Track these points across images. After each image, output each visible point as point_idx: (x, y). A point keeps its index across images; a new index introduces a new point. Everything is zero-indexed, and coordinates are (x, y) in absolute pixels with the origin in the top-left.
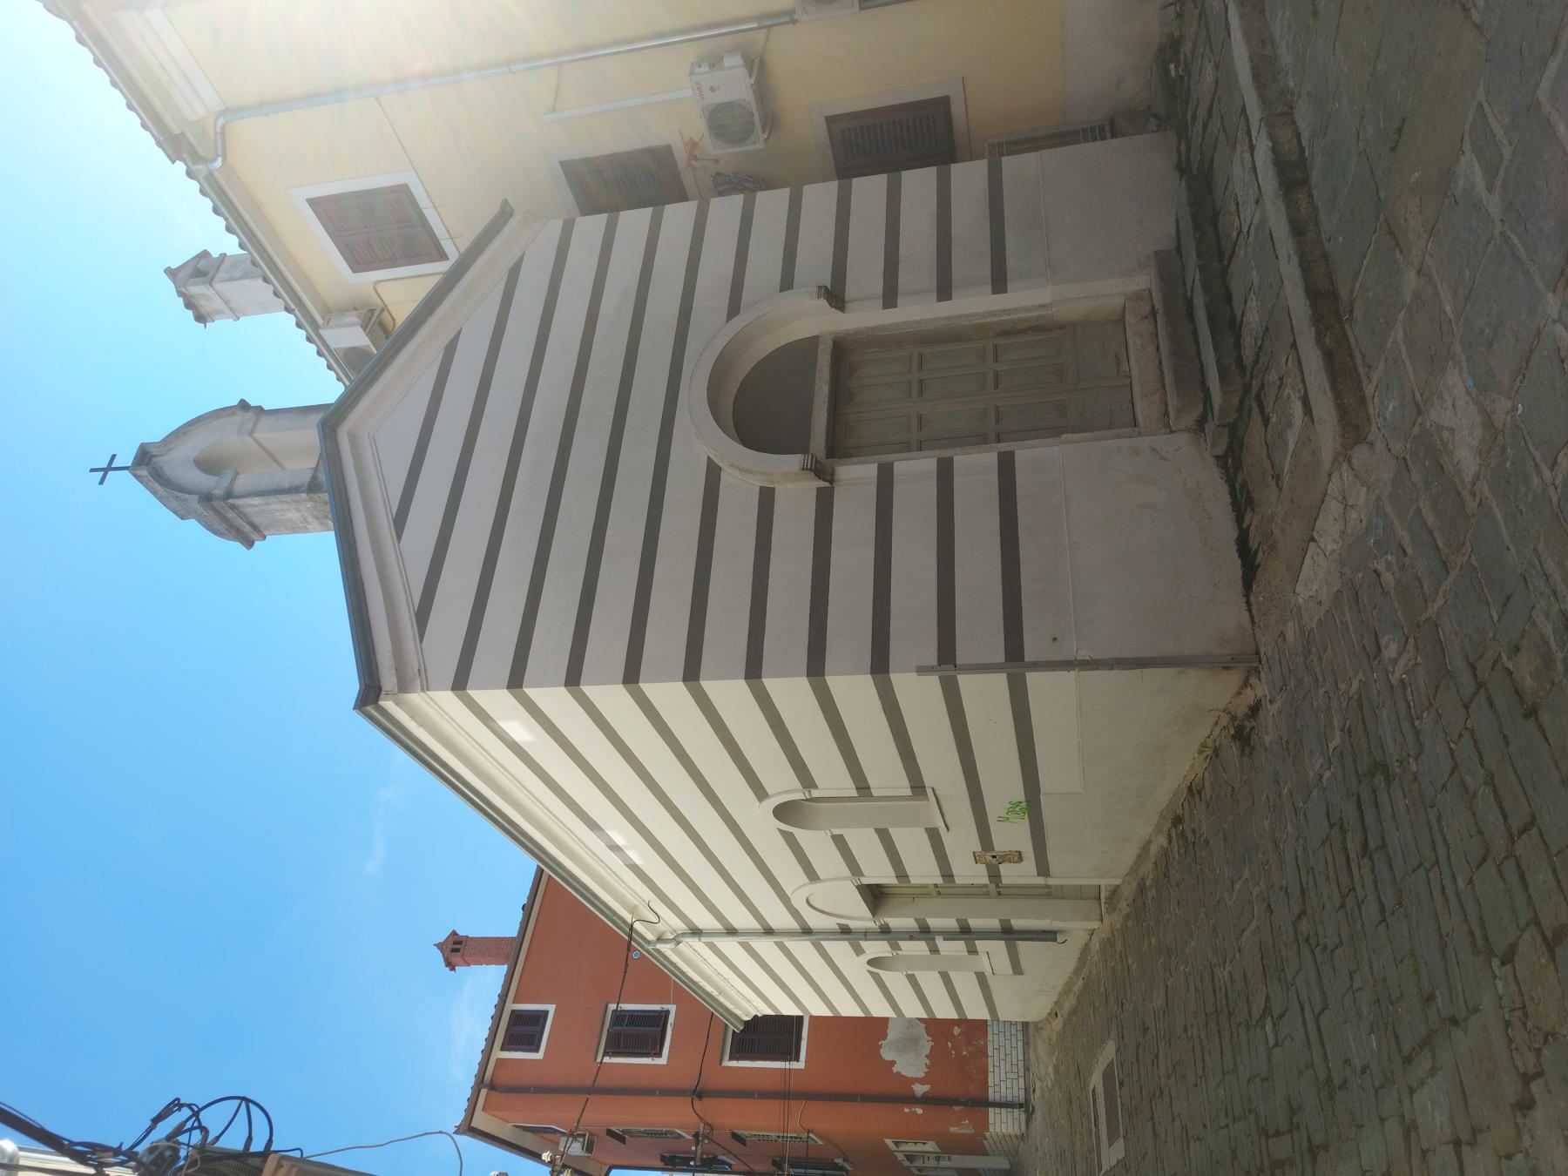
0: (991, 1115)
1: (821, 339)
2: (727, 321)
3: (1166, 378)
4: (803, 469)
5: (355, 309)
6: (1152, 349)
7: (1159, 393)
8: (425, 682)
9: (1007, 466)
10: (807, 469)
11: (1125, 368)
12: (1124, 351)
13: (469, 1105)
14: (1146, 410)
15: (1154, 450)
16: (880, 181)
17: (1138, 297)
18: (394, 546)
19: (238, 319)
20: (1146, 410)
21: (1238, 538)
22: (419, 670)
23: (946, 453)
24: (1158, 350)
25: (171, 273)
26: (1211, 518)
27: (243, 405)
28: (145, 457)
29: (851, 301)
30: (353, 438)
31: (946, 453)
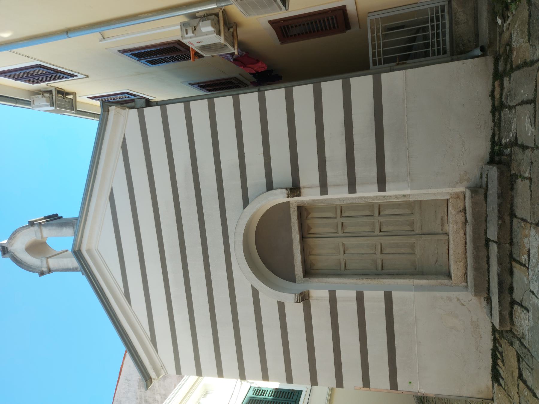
2: (244, 209)
3: (468, 252)
6: (462, 232)
7: (463, 261)
8: (165, 371)
9: (388, 297)
11: (446, 227)
12: (446, 217)
14: (445, 46)
15: (458, 299)
17: (457, 196)
18: (130, 309)
20: (445, 46)
21: (493, 116)
22: (161, 366)
26: (481, 337)
29: (304, 188)
30: (88, 251)
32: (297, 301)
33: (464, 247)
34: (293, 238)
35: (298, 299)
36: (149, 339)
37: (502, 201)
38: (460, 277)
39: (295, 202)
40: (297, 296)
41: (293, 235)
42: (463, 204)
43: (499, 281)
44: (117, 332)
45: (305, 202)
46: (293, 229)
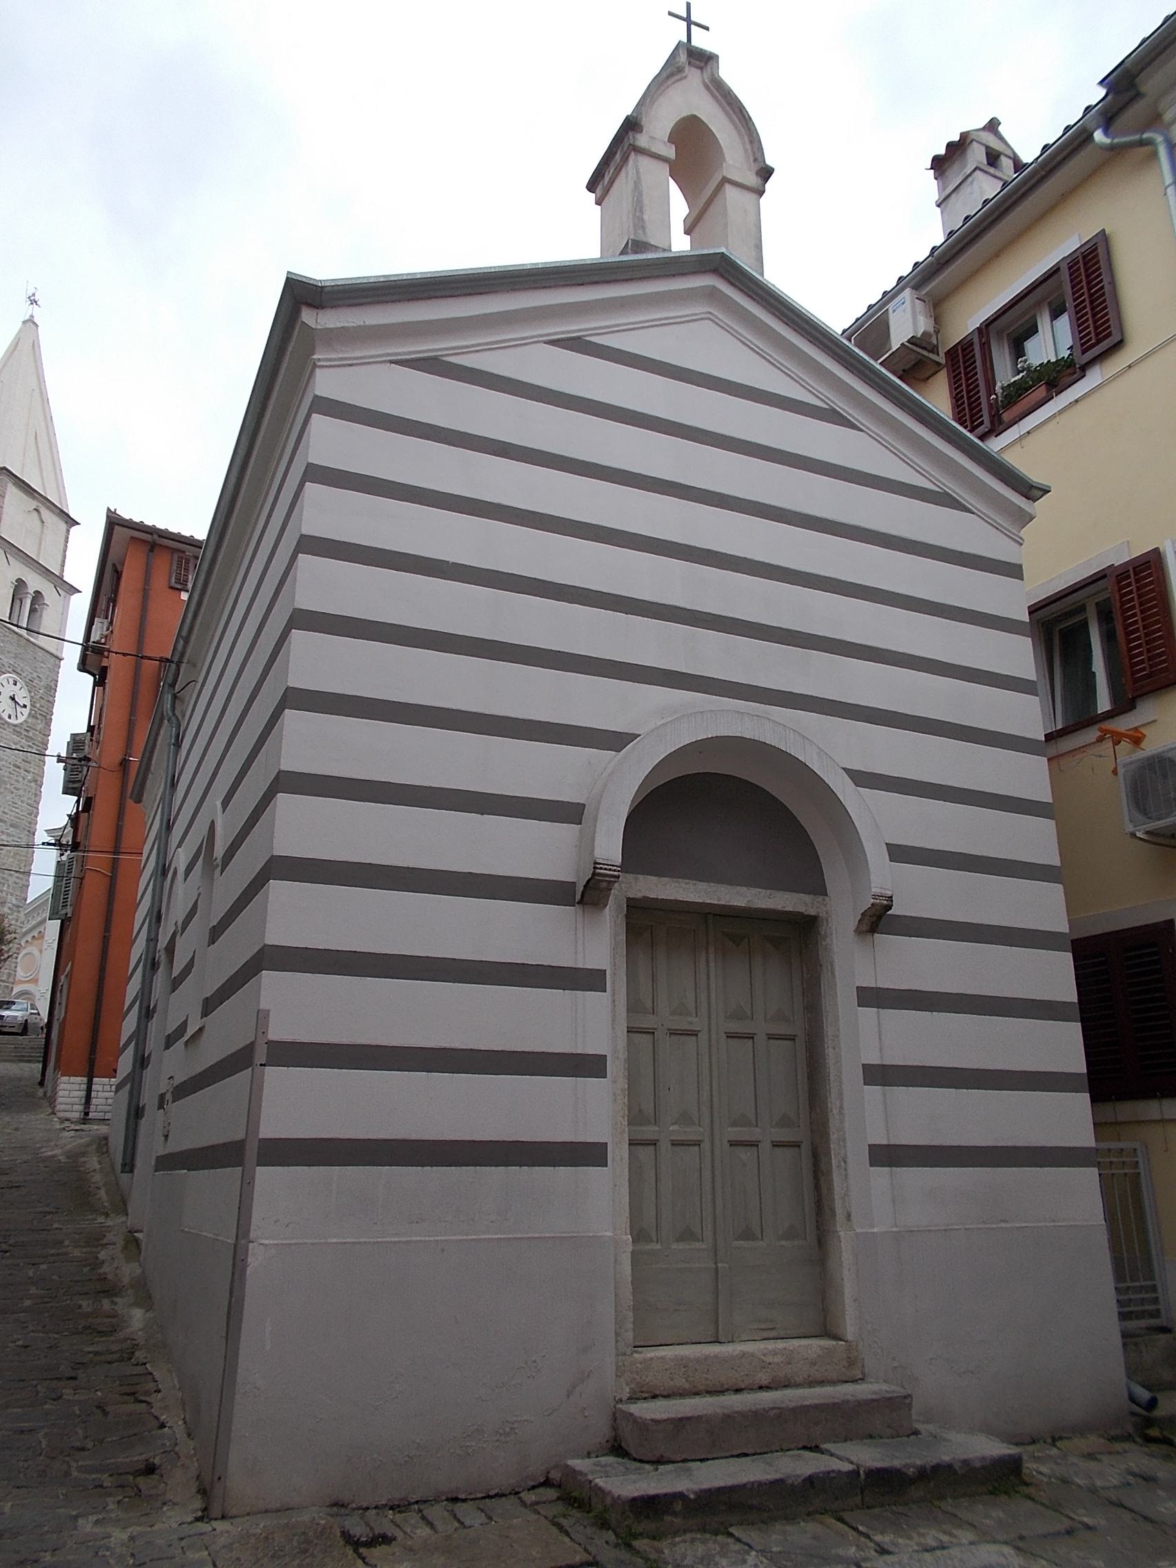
0: (79, 1079)
1: (820, 898)
4: (596, 863)
5: (937, 332)
6: (764, 1378)
10: (595, 868)
13: (135, 523)
16: (1068, 992)
19: (938, 206)
23: (614, 1067)
24: (761, 1388)
25: (993, 125)
27: (766, 173)
28: (703, 60)
31: (614, 1067)
32: (601, 868)
33: (726, 1387)
34: (738, 888)
35: (602, 871)
36: (442, 356)
37: (959, 1472)
38: (644, 1378)
39: (827, 913)
40: (615, 871)
41: (745, 889)
42: (835, 1378)
43: (765, 1483)
44: (1172, 591)
45: (828, 940)
46: (760, 892)
